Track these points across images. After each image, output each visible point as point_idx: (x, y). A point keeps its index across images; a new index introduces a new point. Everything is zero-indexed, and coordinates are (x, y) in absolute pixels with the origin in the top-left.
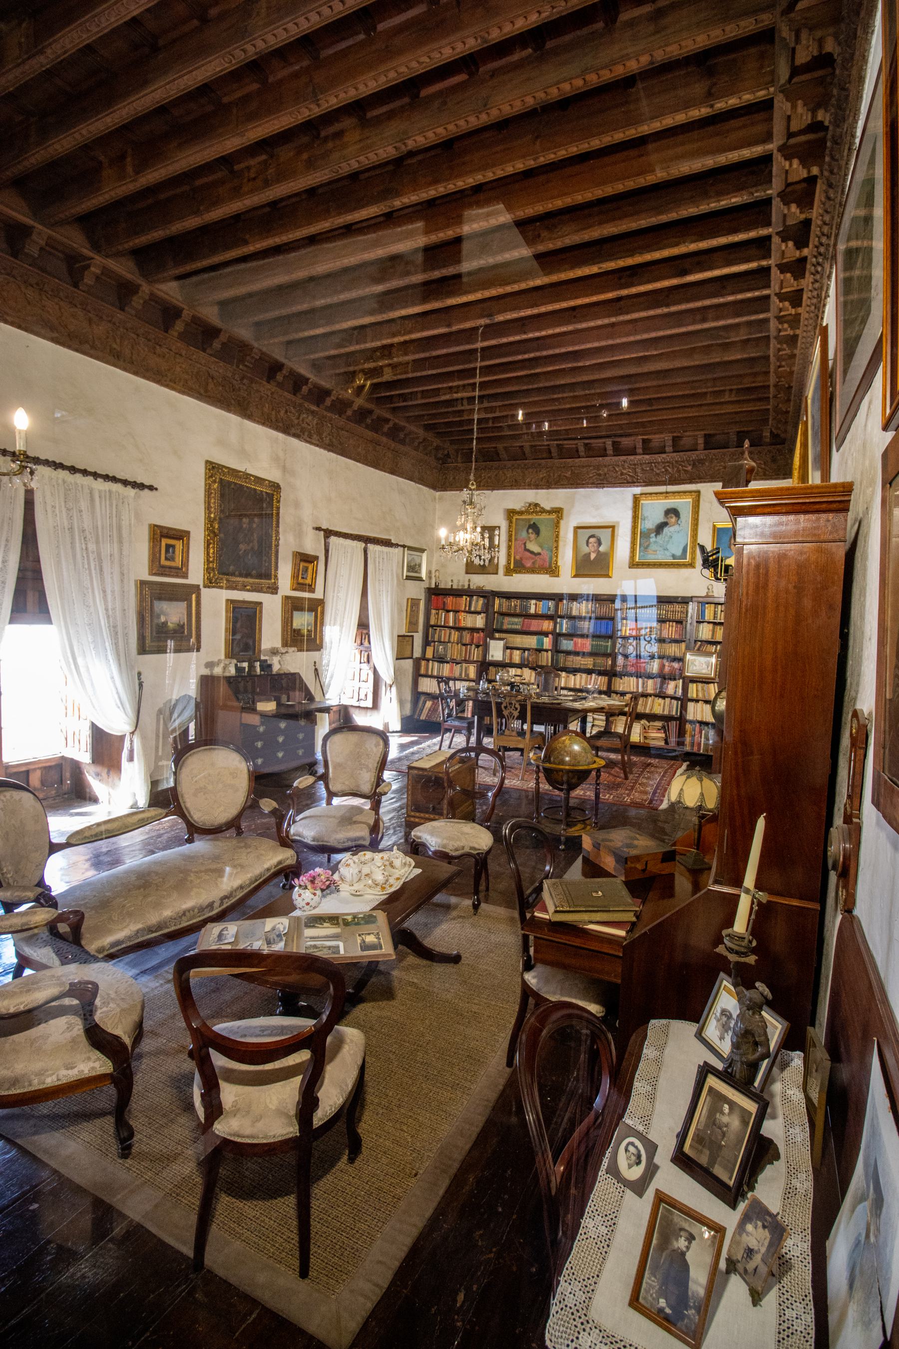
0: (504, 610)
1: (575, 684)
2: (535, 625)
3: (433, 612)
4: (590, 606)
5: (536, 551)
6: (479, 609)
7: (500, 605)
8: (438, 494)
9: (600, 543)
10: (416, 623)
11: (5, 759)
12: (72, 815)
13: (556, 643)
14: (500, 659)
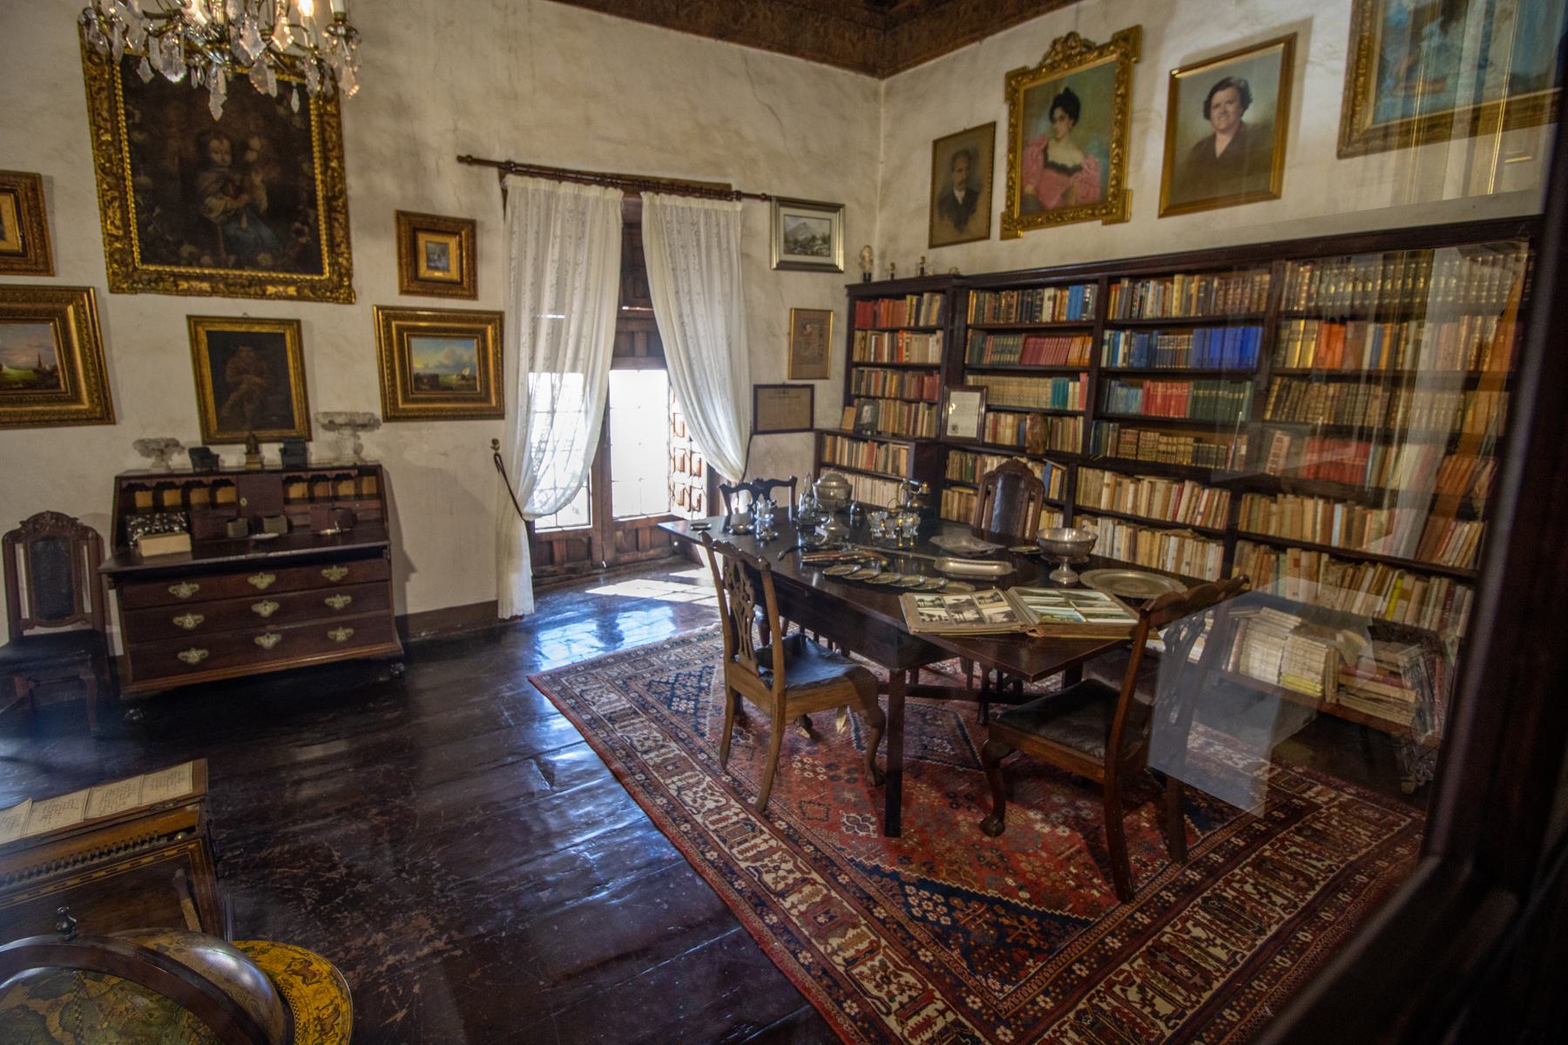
0: (988, 319)
1: (1135, 506)
2: (1050, 351)
3: (858, 334)
4: (1194, 286)
5: (1070, 164)
6: (933, 322)
7: (979, 308)
8: (883, 84)
9: (1244, 99)
10: (822, 357)
11: (615, 514)
12: (668, 579)
13: (1097, 395)
14: (973, 434)
